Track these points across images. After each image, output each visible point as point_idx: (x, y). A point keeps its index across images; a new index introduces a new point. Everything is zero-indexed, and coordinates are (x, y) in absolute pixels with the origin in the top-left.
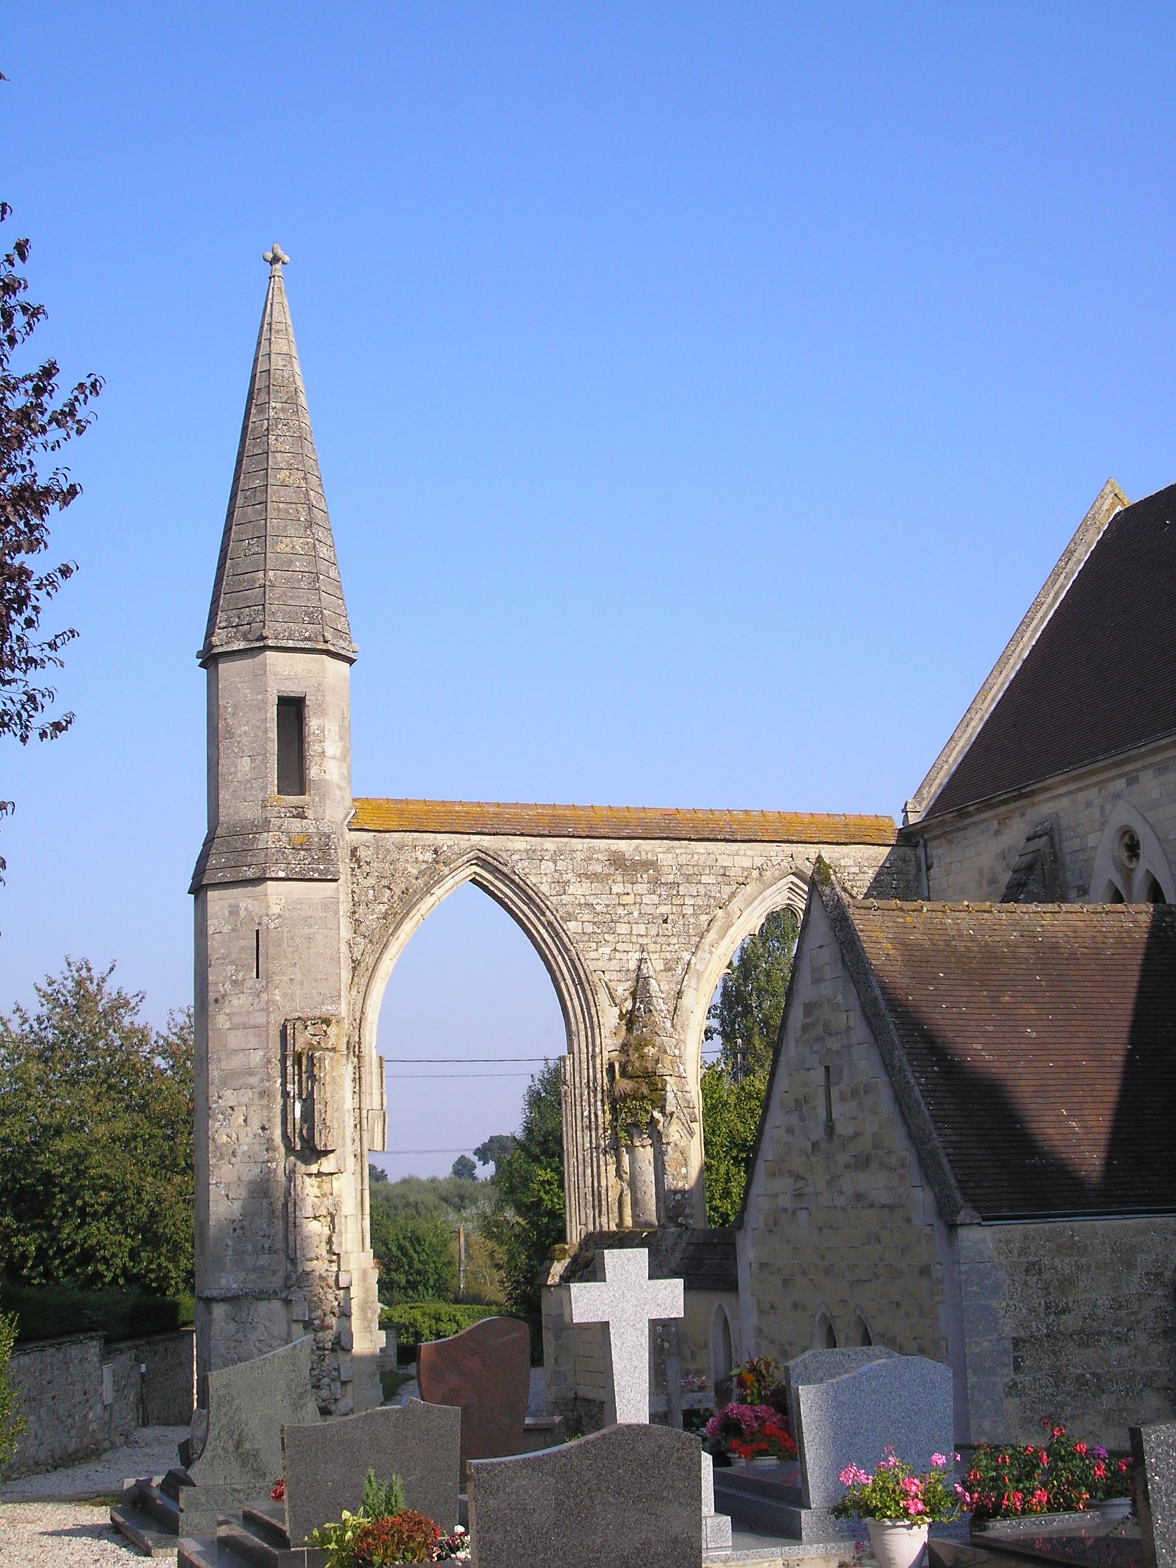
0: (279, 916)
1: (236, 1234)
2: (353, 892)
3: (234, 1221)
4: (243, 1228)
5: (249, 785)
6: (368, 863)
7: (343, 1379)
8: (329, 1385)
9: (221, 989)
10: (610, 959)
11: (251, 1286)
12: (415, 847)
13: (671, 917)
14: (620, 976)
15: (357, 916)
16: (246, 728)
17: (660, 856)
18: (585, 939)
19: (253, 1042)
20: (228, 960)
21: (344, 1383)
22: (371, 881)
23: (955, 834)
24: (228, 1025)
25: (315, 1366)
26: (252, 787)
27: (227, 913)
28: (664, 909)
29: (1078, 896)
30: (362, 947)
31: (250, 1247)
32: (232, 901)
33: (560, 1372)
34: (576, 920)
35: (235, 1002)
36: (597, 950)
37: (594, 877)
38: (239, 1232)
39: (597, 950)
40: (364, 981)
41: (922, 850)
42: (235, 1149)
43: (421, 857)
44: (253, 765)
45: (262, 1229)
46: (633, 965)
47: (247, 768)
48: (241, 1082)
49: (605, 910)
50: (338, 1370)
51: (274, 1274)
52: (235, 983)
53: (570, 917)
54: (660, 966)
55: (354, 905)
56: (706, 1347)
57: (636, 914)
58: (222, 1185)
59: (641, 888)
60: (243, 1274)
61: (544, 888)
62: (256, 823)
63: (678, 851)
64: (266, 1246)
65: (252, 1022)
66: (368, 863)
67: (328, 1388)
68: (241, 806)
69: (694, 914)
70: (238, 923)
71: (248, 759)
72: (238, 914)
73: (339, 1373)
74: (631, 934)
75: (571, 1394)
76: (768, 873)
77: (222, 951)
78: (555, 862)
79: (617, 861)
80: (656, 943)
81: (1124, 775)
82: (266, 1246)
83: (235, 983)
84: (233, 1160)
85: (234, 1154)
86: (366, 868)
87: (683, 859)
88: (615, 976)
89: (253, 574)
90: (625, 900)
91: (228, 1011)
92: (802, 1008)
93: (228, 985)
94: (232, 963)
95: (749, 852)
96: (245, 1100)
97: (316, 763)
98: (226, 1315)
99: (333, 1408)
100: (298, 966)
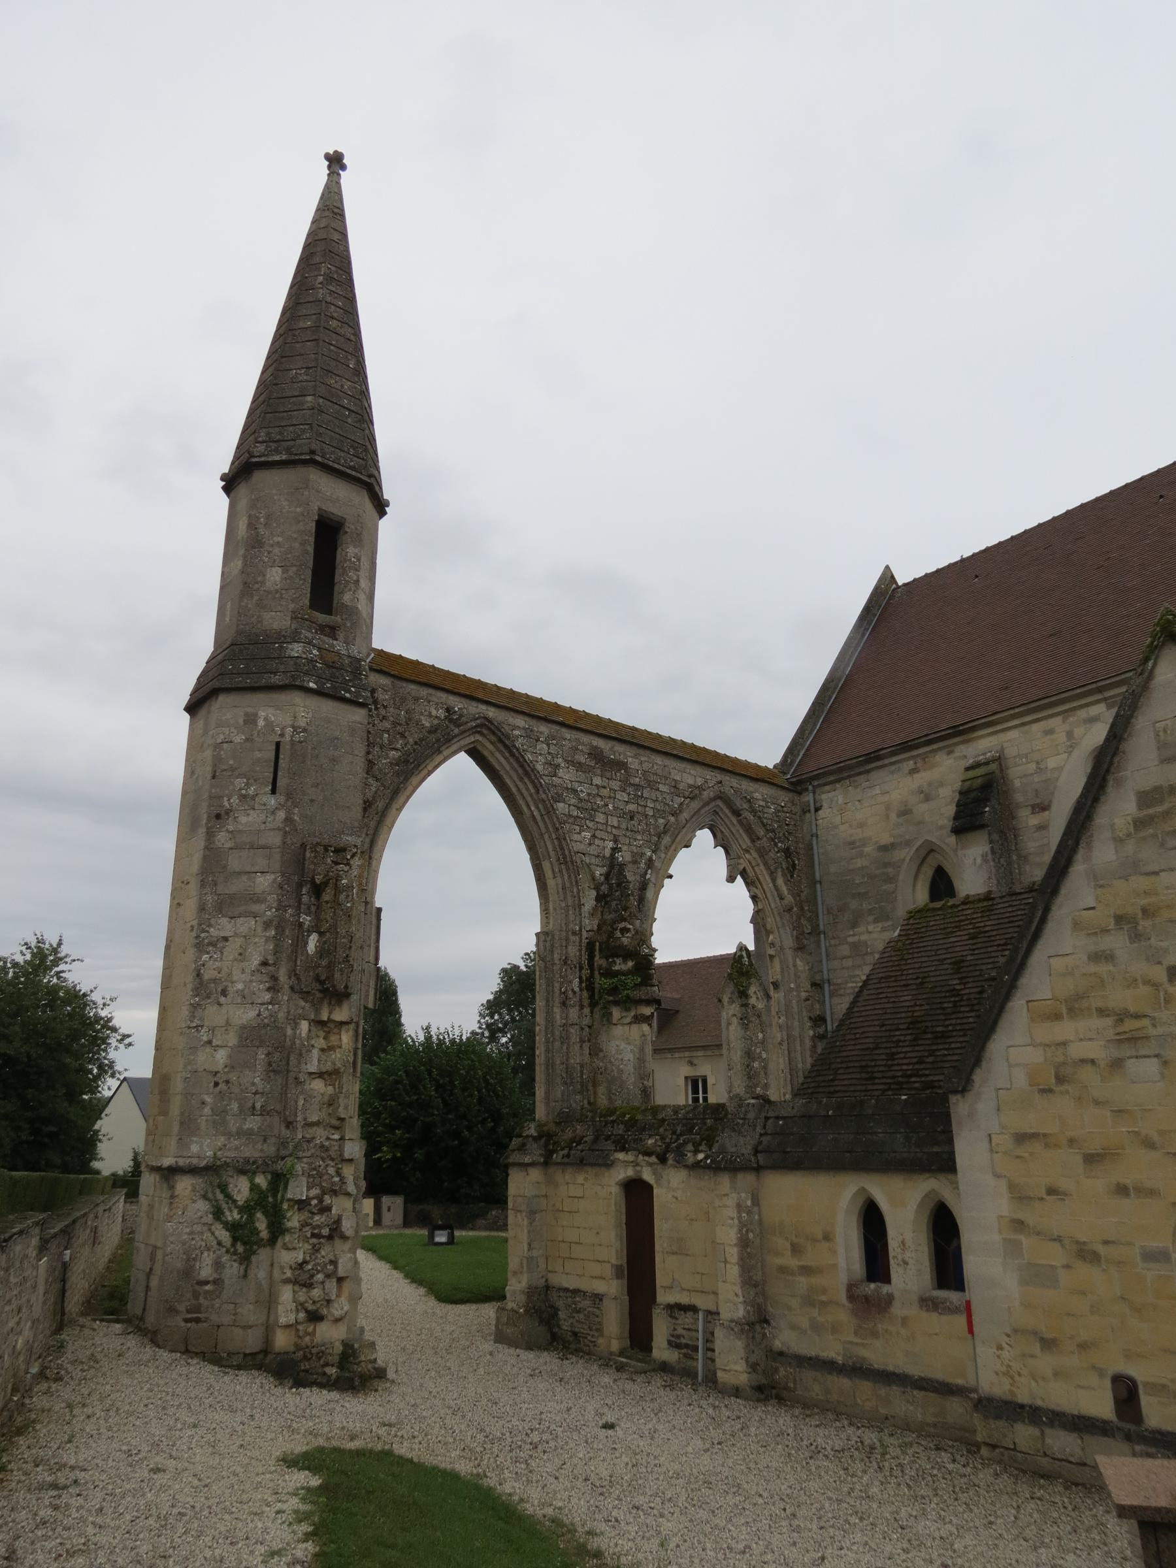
0: (305, 730)
1: (218, 1089)
2: (369, 732)
3: (216, 1073)
4: (227, 1082)
5: (278, 595)
6: (385, 707)
7: (341, 1273)
8: (323, 1283)
9: (226, 804)
10: (590, 844)
11: (232, 1154)
12: (429, 702)
13: (637, 816)
14: (597, 861)
15: (370, 757)
16: (280, 539)
17: (630, 759)
18: (570, 821)
19: (261, 863)
20: (237, 773)
21: (340, 1280)
22: (387, 725)
23: (856, 778)
24: (228, 845)
25: (308, 1258)
26: (281, 597)
27: (241, 721)
28: (631, 807)
29: (1033, 813)
30: (374, 789)
31: (235, 1106)
32: (249, 710)
33: (532, 1258)
34: (564, 802)
35: (243, 819)
36: (580, 833)
37: (579, 766)
38: (222, 1086)
39: (580, 833)
40: (373, 824)
41: (811, 795)
42: (227, 986)
43: (434, 713)
44: (285, 576)
45: (253, 1084)
46: (607, 853)
47: (278, 578)
48: (242, 909)
49: (586, 798)
50: (334, 1263)
51: (265, 1140)
52: (243, 798)
53: (559, 798)
54: (628, 858)
55: (368, 745)
56: (827, 1237)
57: (611, 807)
58: (205, 1029)
59: (615, 785)
60: (222, 1139)
61: (539, 767)
62: (283, 633)
63: (643, 759)
64: (258, 1105)
65: (262, 842)
66: (385, 707)
67: (321, 1286)
68: (267, 616)
69: (653, 816)
70: (255, 733)
71: (280, 570)
72: (255, 722)
73: (336, 1267)
74: (606, 824)
75: (542, 1282)
76: (705, 793)
77: (231, 762)
78: (548, 745)
79: (596, 755)
80: (625, 836)
81: (1105, 699)
82: (258, 1105)
83: (243, 798)
84: (222, 999)
85: (224, 993)
86: (383, 712)
87: (646, 766)
88: (593, 860)
89: (300, 398)
90: (605, 792)
91: (231, 828)
92: (1133, 798)
93: (235, 800)
94: (241, 775)
95: (693, 772)
96: (243, 929)
97: (350, 590)
98: (194, 1190)
99: (325, 1311)
100: (320, 787)
